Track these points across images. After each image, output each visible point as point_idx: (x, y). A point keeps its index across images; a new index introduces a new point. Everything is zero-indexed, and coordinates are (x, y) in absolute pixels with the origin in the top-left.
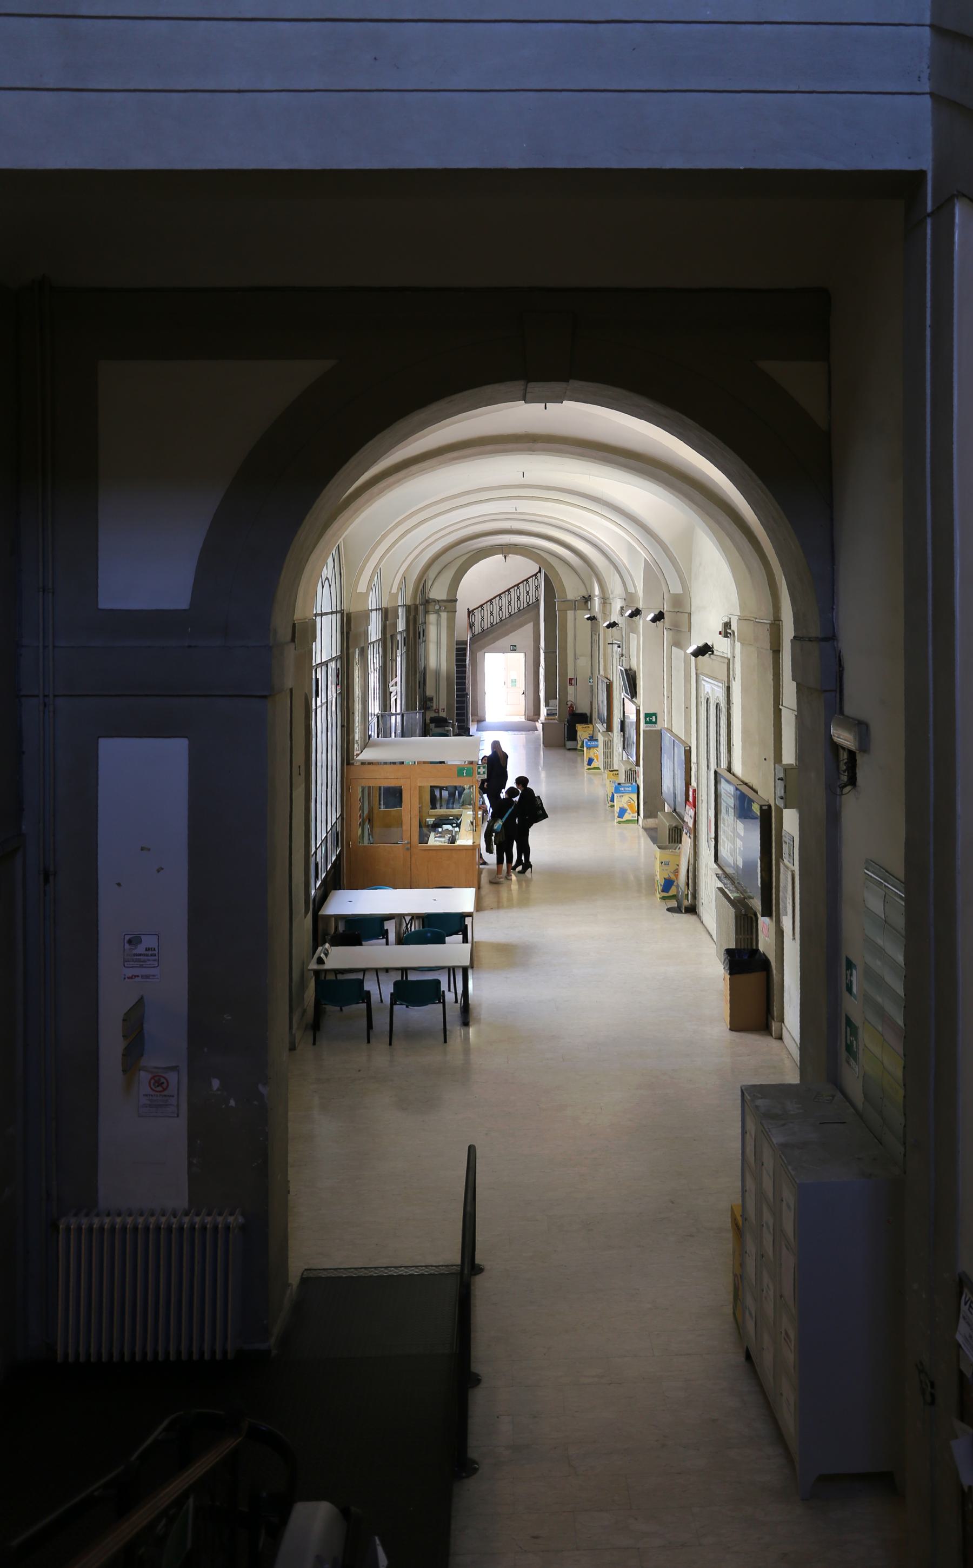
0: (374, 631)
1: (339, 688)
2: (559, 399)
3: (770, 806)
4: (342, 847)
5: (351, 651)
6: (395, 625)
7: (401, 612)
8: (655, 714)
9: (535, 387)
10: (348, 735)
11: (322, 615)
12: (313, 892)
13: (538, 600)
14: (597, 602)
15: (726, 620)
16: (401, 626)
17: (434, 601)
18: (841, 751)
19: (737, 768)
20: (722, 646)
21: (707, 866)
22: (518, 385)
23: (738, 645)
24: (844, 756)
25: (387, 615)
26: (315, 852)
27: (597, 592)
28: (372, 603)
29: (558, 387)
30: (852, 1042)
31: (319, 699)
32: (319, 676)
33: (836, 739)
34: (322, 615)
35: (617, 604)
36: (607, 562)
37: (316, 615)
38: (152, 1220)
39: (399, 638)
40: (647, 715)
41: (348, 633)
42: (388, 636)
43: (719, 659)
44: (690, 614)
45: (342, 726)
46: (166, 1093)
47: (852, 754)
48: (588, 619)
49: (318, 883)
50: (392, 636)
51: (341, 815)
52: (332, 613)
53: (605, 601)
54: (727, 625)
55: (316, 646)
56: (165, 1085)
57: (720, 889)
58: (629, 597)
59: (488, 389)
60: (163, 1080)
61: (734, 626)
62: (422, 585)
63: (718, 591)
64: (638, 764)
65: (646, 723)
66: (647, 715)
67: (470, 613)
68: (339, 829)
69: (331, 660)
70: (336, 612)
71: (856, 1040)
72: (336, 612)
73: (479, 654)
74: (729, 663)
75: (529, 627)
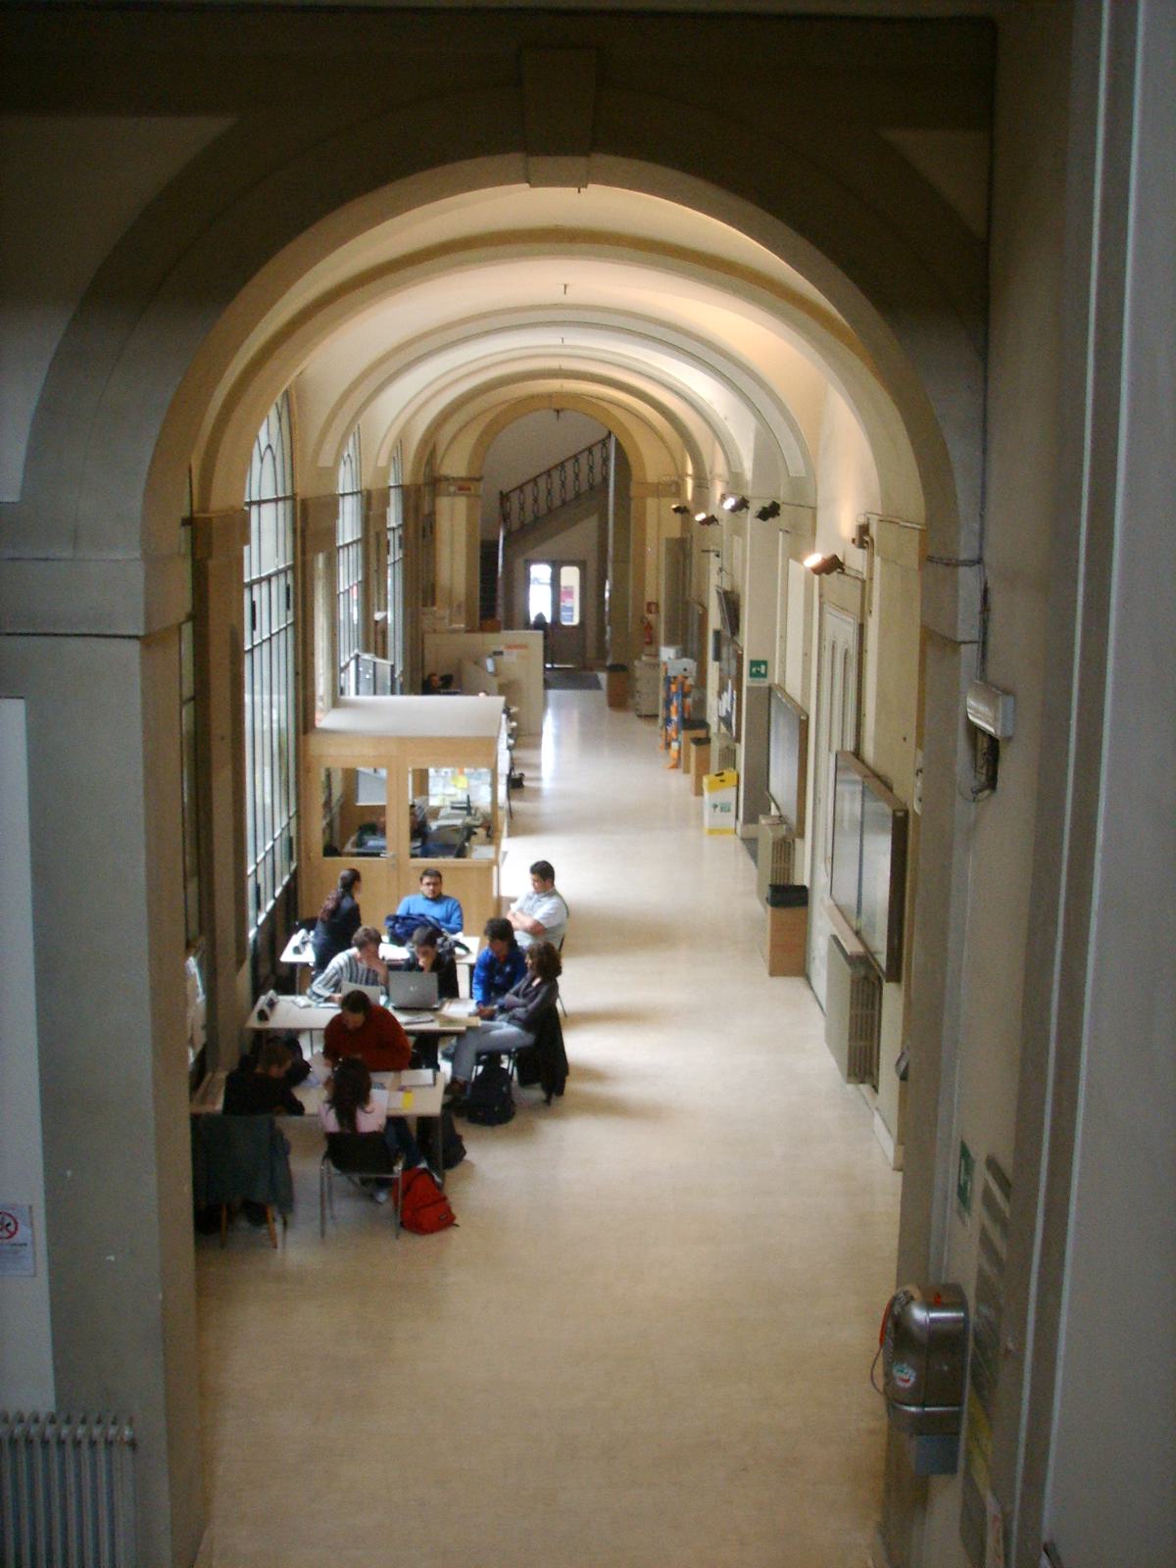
0: (348, 527)
1: (290, 613)
2: (580, 182)
3: (906, 813)
4: (299, 860)
5: (309, 557)
6: (383, 517)
7: (395, 497)
8: (765, 663)
9: (539, 163)
10: (305, 687)
11: (260, 503)
12: (252, 933)
13: (605, 480)
14: (690, 483)
15: (862, 520)
16: (393, 518)
17: (447, 479)
18: (980, 735)
19: (869, 751)
20: (856, 559)
21: (822, 899)
22: (515, 159)
23: (877, 560)
24: (983, 744)
25: (371, 504)
26: (256, 871)
27: (690, 470)
28: (345, 481)
29: (579, 163)
30: (966, 1183)
31: (256, 633)
32: (256, 598)
33: (971, 717)
34: (260, 503)
35: (718, 489)
36: (699, 420)
37: (250, 504)
38: (18, 1430)
39: (390, 535)
40: (754, 663)
41: (303, 531)
42: (372, 534)
43: (851, 581)
44: (814, 509)
45: (297, 674)
46: (14, 1240)
47: (994, 743)
48: (677, 510)
49: (262, 917)
50: (378, 535)
51: (297, 812)
52: (276, 500)
53: (702, 483)
54: (864, 530)
55: (250, 553)
56: (12, 1228)
57: (835, 938)
58: (735, 480)
59: (467, 166)
60: (8, 1220)
61: (873, 530)
62: (429, 452)
63: (851, 472)
64: (738, 739)
65: (752, 675)
66: (754, 663)
67: (504, 497)
68: (293, 833)
69: (277, 574)
70: (284, 499)
71: (971, 1180)
72: (284, 499)
73: (519, 562)
74: (865, 585)
75: (591, 524)
